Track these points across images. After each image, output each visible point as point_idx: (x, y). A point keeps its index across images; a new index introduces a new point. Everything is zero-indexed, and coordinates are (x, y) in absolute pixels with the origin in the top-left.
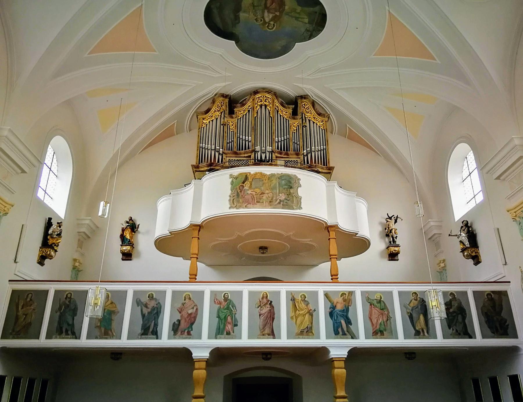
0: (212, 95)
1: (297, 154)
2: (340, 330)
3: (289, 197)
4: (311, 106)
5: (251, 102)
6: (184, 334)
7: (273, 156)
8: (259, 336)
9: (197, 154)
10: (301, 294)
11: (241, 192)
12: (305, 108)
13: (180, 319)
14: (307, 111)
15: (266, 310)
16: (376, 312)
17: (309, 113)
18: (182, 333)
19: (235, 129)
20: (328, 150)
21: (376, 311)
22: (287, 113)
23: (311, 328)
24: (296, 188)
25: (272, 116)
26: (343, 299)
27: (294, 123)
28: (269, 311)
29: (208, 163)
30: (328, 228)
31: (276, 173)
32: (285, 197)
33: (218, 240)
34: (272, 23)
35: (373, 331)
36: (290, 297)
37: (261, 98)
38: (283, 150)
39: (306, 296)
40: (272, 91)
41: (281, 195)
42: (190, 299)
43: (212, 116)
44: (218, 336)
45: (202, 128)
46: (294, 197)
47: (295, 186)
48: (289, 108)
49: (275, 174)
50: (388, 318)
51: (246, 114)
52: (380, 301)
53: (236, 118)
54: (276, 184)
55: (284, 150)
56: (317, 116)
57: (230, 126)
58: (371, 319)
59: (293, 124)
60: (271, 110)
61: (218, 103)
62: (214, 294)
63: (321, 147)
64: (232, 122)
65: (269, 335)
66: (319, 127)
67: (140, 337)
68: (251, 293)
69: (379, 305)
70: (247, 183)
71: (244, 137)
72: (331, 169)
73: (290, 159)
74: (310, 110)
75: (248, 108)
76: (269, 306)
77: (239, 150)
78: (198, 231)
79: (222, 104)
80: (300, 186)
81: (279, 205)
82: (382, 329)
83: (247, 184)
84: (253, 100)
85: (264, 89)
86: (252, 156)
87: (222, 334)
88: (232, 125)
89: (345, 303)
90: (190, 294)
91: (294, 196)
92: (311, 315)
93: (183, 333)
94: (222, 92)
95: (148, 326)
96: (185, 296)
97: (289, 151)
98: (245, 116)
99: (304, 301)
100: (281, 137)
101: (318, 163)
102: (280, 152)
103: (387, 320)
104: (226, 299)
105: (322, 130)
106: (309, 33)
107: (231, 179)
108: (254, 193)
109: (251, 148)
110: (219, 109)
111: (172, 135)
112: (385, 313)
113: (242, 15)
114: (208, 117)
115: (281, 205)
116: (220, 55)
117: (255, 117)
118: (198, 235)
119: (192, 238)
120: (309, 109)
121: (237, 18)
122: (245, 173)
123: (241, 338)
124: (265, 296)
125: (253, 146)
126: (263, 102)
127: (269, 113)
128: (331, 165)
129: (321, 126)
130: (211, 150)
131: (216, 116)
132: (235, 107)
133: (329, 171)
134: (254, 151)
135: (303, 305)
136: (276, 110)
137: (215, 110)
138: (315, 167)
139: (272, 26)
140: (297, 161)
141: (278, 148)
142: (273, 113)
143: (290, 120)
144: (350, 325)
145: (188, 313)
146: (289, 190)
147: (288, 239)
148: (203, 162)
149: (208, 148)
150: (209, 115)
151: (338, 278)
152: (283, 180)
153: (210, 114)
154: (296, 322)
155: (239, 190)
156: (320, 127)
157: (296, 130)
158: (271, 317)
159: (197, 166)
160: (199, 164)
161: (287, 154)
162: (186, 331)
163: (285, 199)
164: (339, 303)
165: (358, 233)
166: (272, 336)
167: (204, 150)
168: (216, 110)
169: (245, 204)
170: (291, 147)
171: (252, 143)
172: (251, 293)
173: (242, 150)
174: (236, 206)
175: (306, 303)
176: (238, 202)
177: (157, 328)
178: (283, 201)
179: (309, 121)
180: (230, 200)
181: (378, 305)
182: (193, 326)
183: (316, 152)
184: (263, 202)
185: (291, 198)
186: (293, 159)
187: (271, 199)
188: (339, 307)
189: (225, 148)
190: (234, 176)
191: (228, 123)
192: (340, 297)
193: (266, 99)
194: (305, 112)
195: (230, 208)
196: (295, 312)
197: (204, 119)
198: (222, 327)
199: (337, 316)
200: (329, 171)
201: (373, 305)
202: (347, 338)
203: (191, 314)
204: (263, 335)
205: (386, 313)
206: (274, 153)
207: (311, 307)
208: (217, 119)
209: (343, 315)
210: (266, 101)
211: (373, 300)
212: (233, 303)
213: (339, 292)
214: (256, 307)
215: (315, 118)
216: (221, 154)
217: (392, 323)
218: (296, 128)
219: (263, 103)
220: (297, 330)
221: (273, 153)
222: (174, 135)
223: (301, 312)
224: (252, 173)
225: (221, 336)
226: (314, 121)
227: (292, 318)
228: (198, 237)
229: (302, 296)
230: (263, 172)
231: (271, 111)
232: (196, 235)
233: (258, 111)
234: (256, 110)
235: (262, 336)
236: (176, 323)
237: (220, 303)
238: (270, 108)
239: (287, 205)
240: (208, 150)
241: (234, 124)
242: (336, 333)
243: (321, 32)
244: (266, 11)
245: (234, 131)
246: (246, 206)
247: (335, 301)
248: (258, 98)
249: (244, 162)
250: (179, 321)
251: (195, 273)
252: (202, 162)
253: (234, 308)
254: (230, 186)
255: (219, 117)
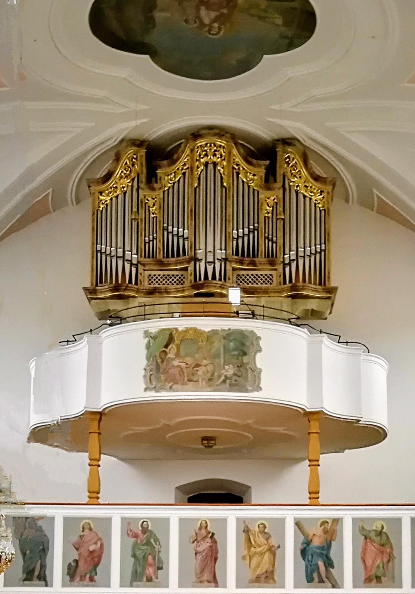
0: (115, 141)
1: (272, 263)
2: (315, 575)
3: (240, 371)
4: (300, 162)
5: (187, 156)
6: (85, 580)
7: (229, 268)
8: (195, 584)
9: (92, 265)
10: (259, 523)
11: (162, 362)
12: (291, 165)
13: (77, 558)
14: (293, 172)
15: (205, 545)
16: (372, 549)
17: (297, 178)
18: (82, 578)
19: (160, 212)
20: (329, 251)
21: (373, 548)
22: (256, 177)
23: (272, 572)
24: (253, 354)
25: (227, 185)
26: (323, 529)
27: (268, 198)
28: (209, 548)
29: (112, 286)
30: (309, 415)
31: (219, 329)
32: (234, 371)
33: (132, 430)
34: (216, 25)
35: (366, 577)
36: (242, 527)
37: (206, 148)
38: (246, 256)
39: (267, 525)
40: (227, 133)
41: (226, 367)
42: (91, 529)
43: (116, 187)
44: (135, 583)
45: (99, 212)
46: (250, 371)
47: (251, 353)
48: (260, 166)
49: (217, 330)
50: (391, 557)
51: (179, 181)
52: (380, 533)
53: (160, 189)
54: (220, 347)
55: (248, 255)
56: (312, 183)
57: (149, 207)
58: (364, 562)
59: (266, 200)
60: (226, 173)
61: (125, 160)
62: (126, 522)
63: (317, 246)
64: (153, 199)
65: (209, 582)
66: (315, 204)
67: (21, 583)
68: (182, 521)
69: (379, 538)
70: (172, 347)
71: (175, 229)
72: (332, 292)
73: (259, 273)
74: (299, 171)
75: (182, 169)
76: (210, 541)
77: (168, 257)
78: (97, 422)
79: (134, 160)
80: (260, 350)
81: (223, 386)
82: (379, 575)
83: (173, 348)
84: (192, 151)
85: (211, 128)
86: (189, 268)
87: (140, 580)
88: (154, 205)
89: (325, 536)
90: (90, 522)
91: (250, 368)
92: (274, 555)
93: (83, 578)
94: (134, 136)
95: (31, 568)
96: (83, 526)
97: (258, 257)
98: (176, 185)
99: (263, 533)
100: (243, 229)
101: (310, 282)
102: (241, 260)
103: (389, 561)
104: (145, 530)
105: (320, 211)
106: (287, 41)
107: (147, 339)
108: (183, 365)
109: (188, 255)
110: (128, 172)
111: (47, 212)
112: (386, 551)
113: (158, 15)
114: (108, 189)
115: (227, 385)
116: (125, 79)
117: (195, 189)
118: (99, 429)
119: (90, 433)
120: (297, 169)
121: (150, 21)
122: (169, 329)
123: (167, 586)
124: (204, 525)
125: (191, 248)
126: (209, 158)
127: (222, 178)
128: (333, 283)
129: (319, 203)
130: (117, 257)
131: (124, 187)
132: (159, 167)
133: (328, 295)
134: (196, 260)
135: (261, 539)
136: (234, 171)
137: (121, 174)
138: (303, 289)
139: (217, 30)
140: (271, 275)
141: (237, 254)
142: (228, 180)
143: (261, 191)
144: (331, 569)
145: (88, 550)
146: (240, 358)
147: (247, 427)
148: (103, 283)
149: (110, 254)
150: (111, 185)
151: (318, 498)
152: (231, 341)
153: (111, 183)
154: (250, 562)
155: (159, 358)
156: (317, 205)
157: (271, 212)
158: (213, 557)
159: (93, 290)
160: (97, 285)
161: (253, 264)
162: (88, 576)
163: (235, 374)
164: (317, 536)
165: (360, 421)
166: (213, 584)
167: (104, 256)
168: (123, 174)
169: (169, 383)
170: (262, 248)
171: (189, 242)
172: (182, 521)
173: (173, 256)
174: (155, 387)
175: (266, 536)
176: (158, 379)
177: (45, 571)
178: (230, 378)
179: (297, 193)
180: (145, 376)
181: (377, 539)
182: (98, 569)
183: (306, 257)
184: (198, 381)
185: (244, 372)
186: (264, 273)
187: (211, 376)
188: (316, 542)
189: (141, 252)
190: (151, 333)
191: (146, 201)
192: (319, 526)
193: (215, 151)
194: (289, 174)
195: (146, 390)
196: (249, 549)
197: (101, 193)
198: (139, 570)
199: (312, 555)
200: (328, 294)
201: (370, 539)
202: (326, 587)
203: (92, 552)
204: (201, 582)
205: (388, 550)
206: (230, 262)
207: (274, 542)
208: (125, 193)
209: (322, 554)
210: (215, 155)
211: (370, 531)
212: (155, 535)
213: (319, 519)
214: (190, 542)
215: (306, 186)
216: (134, 264)
217: (396, 567)
218: (271, 208)
219: (211, 158)
220: (250, 575)
221: (228, 263)
222: (50, 212)
223: (258, 550)
224: (180, 329)
225: (139, 583)
226: (306, 194)
227: (244, 558)
228: (99, 432)
229: (261, 526)
230: (199, 327)
231: (224, 174)
232: (95, 429)
233: (200, 175)
234: (196, 173)
235: (199, 584)
236: (72, 564)
237: (136, 536)
238: (222, 168)
239: (236, 385)
240: (111, 257)
241: (158, 202)
242: (310, 580)
243: (308, 39)
244: (203, 8)
245: (157, 217)
246: (171, 388)
247: (310, 534)
248: (200, 147)
249: (175, 280)
250: (76, 561)
251: (96, 489)
252: (101, 282)
253: (158, 543)
254: (144, 352)
255: (130, 188)
